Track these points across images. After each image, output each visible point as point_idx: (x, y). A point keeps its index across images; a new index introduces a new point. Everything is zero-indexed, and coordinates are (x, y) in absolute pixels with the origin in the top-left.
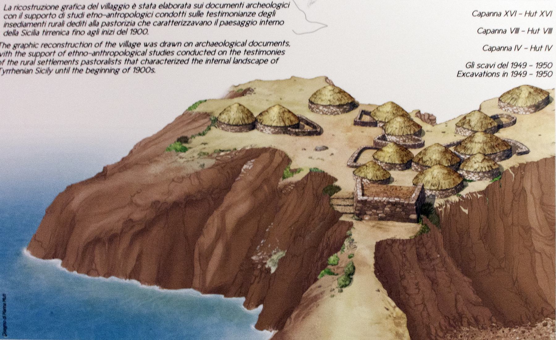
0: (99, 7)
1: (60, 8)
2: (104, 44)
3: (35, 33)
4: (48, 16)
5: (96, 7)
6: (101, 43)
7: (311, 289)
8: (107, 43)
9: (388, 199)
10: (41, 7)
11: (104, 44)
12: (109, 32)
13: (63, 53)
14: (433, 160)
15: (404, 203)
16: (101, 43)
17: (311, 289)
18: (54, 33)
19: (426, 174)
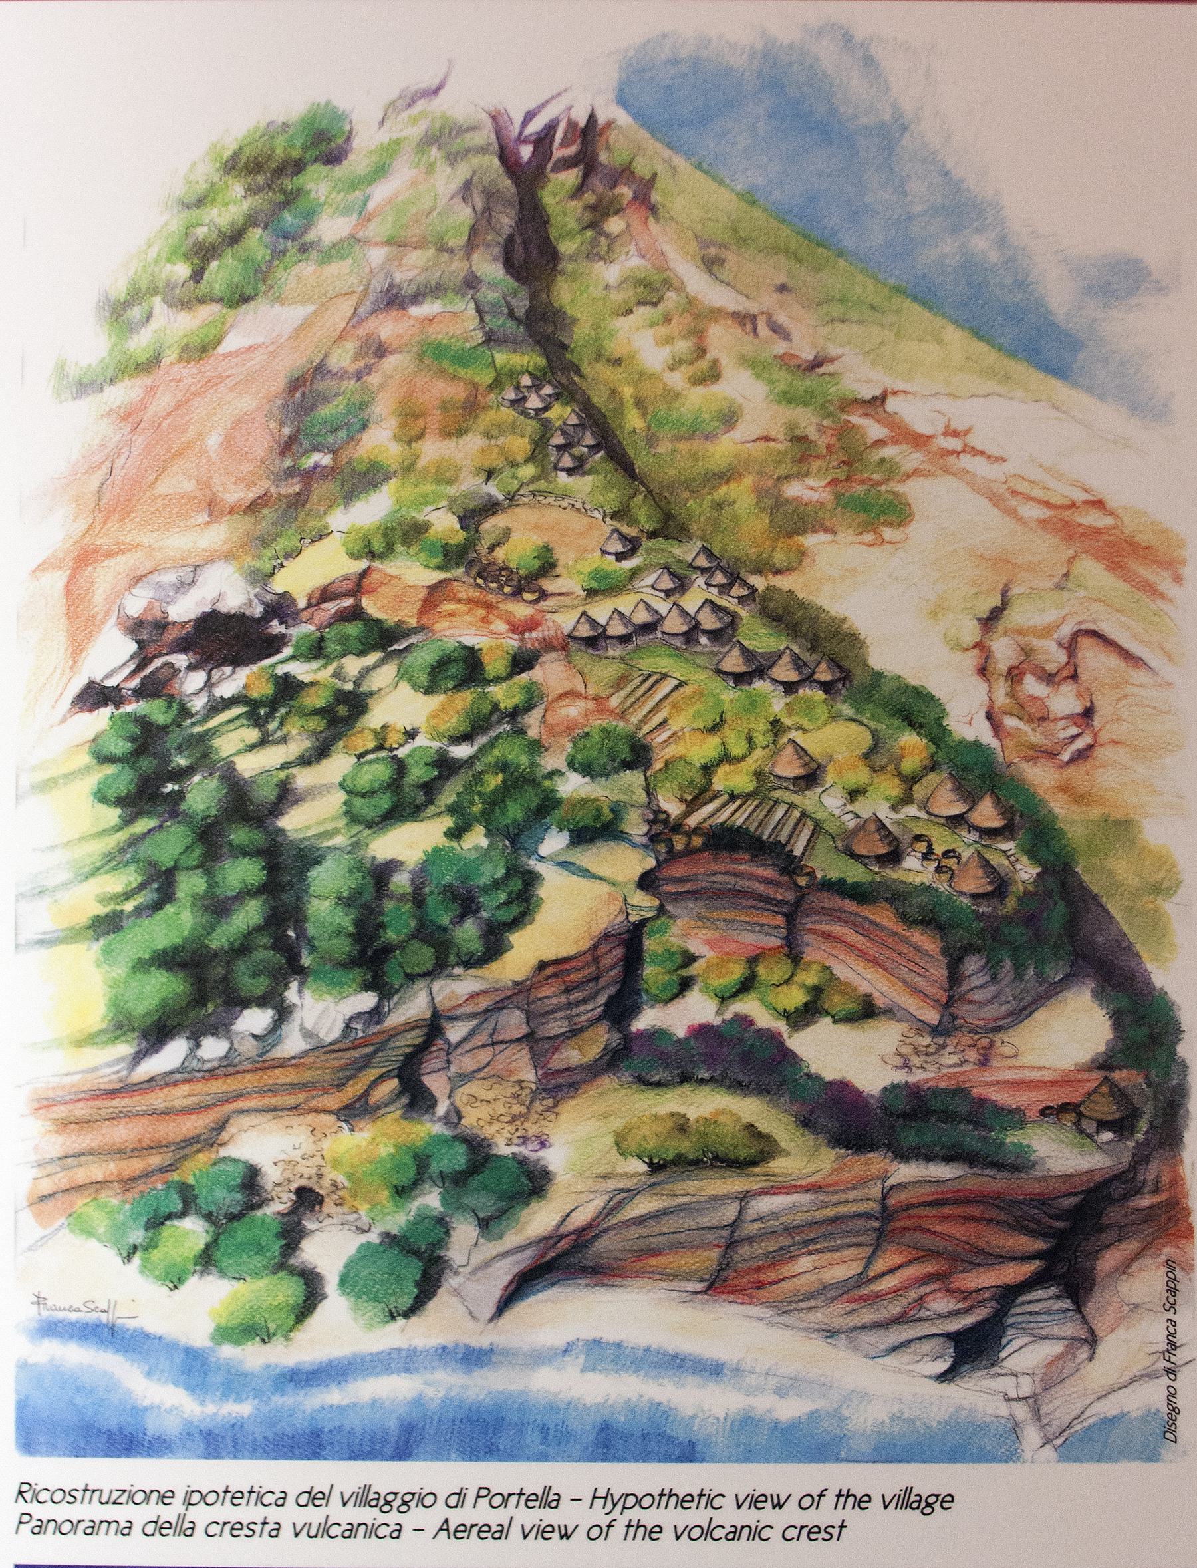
0: (335, 1500)
1: (180, 1496)
2: (830, 1499)
3: (314, 1498)
4: (513, 1499)
5: (325, 1497)
6: (821, 1495)
7: (249, 486)
8: (839, 1496)
9: (631, 401)
10: (116, 1495)
11: (830, 1499)
12: (124, 1499)
13: (816, 1499)
14: (299, 181)
15: (196, 1039)
16: (821, 1495)
17: (249, 486)
18: (257, 1496)
19: (392, 1423)
